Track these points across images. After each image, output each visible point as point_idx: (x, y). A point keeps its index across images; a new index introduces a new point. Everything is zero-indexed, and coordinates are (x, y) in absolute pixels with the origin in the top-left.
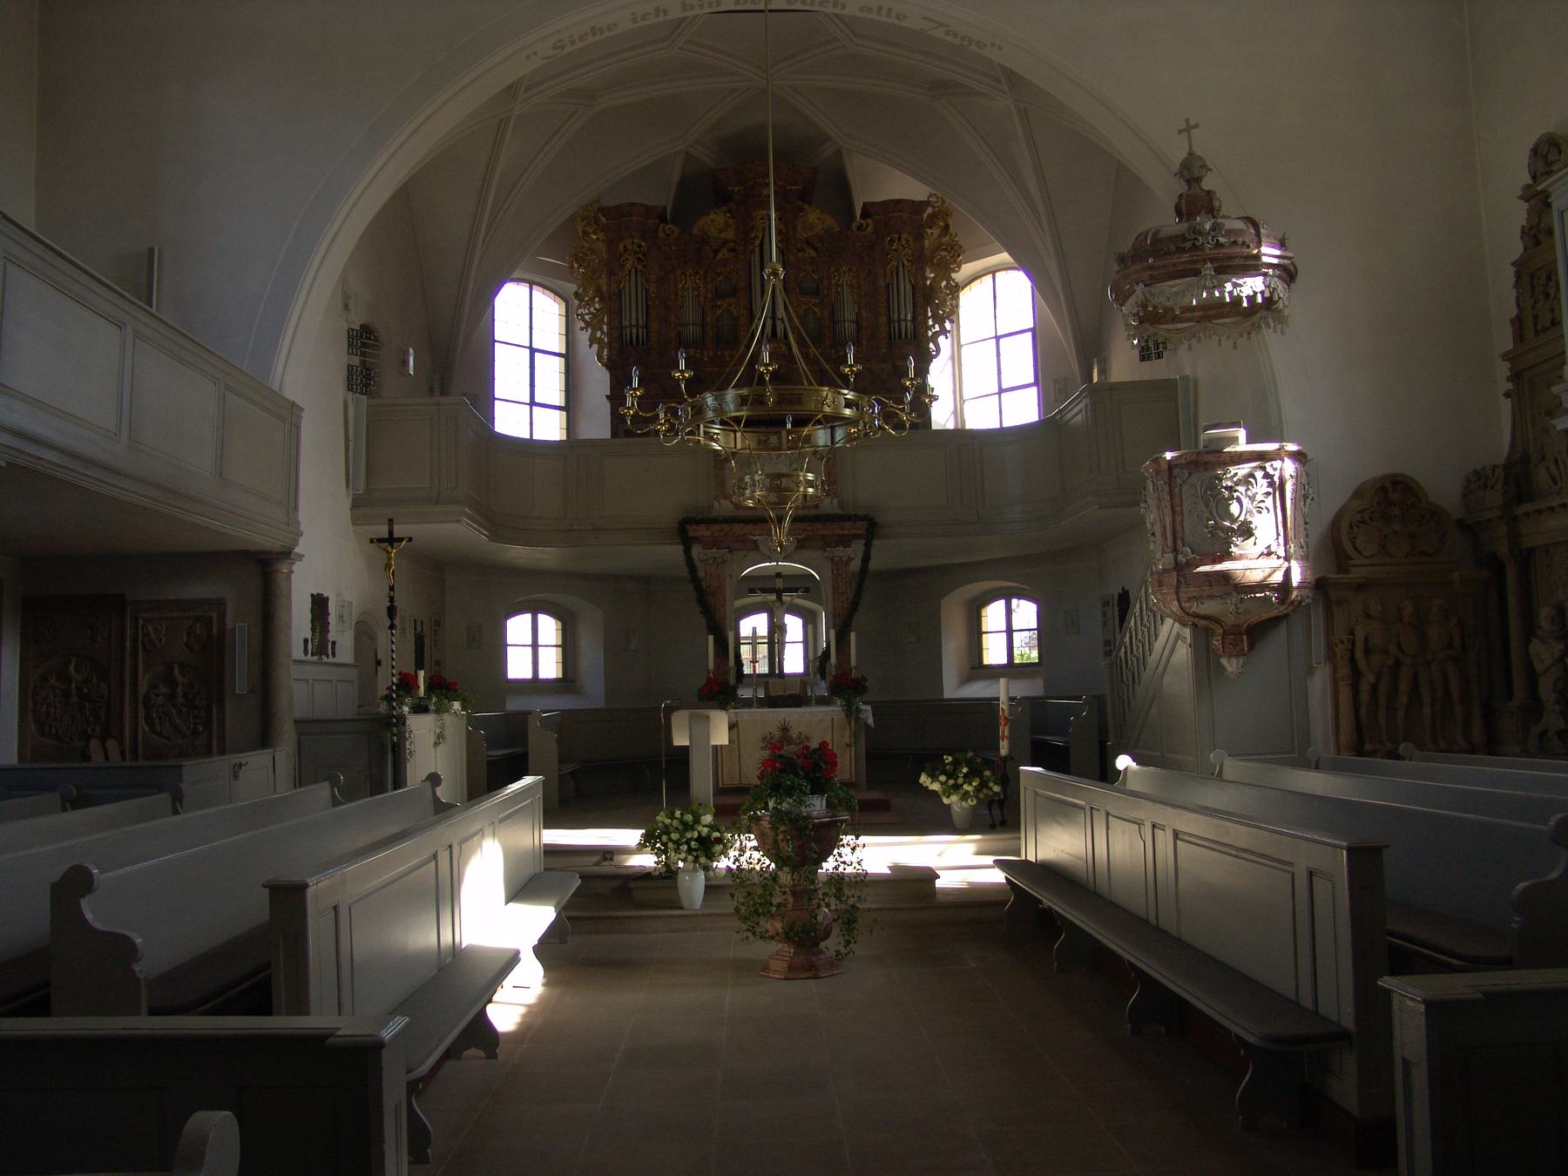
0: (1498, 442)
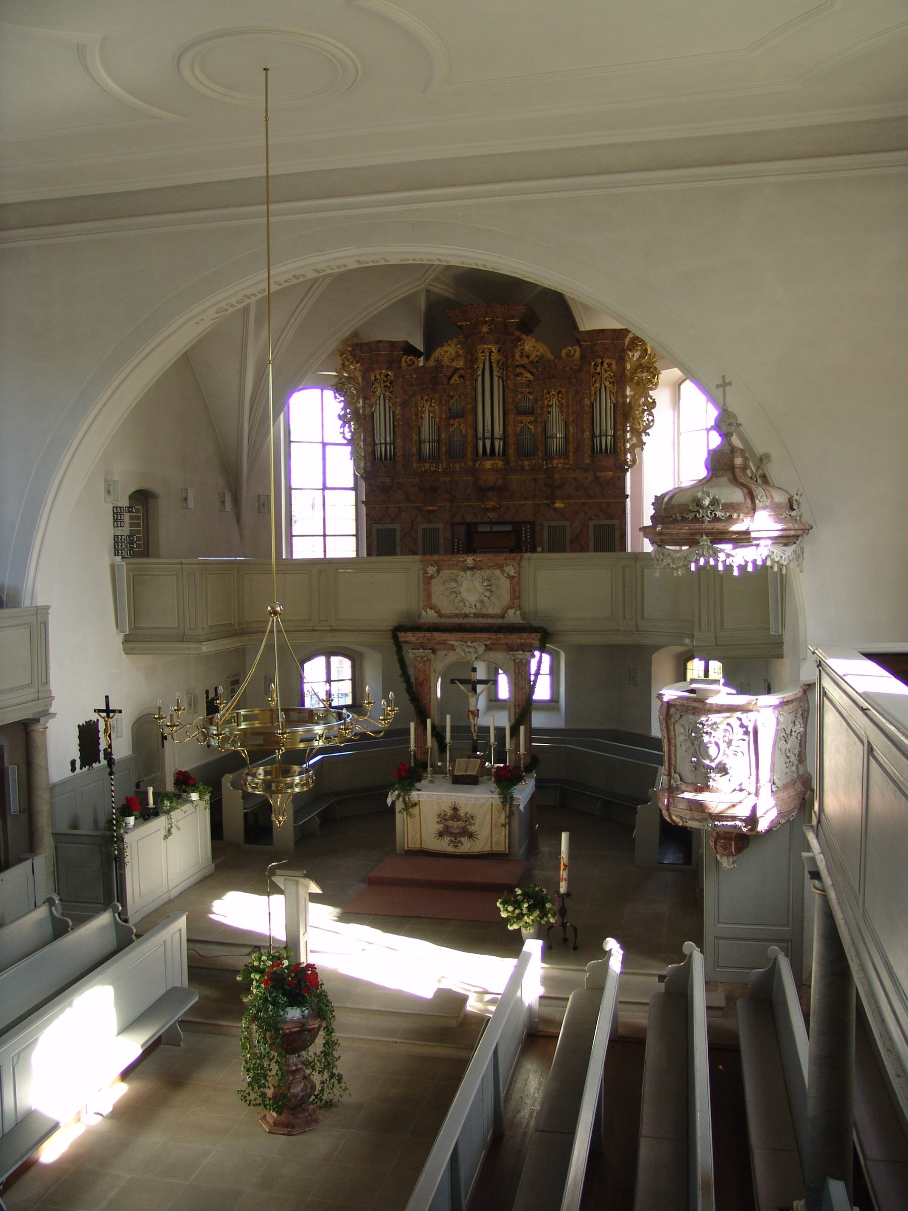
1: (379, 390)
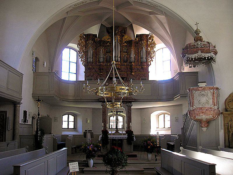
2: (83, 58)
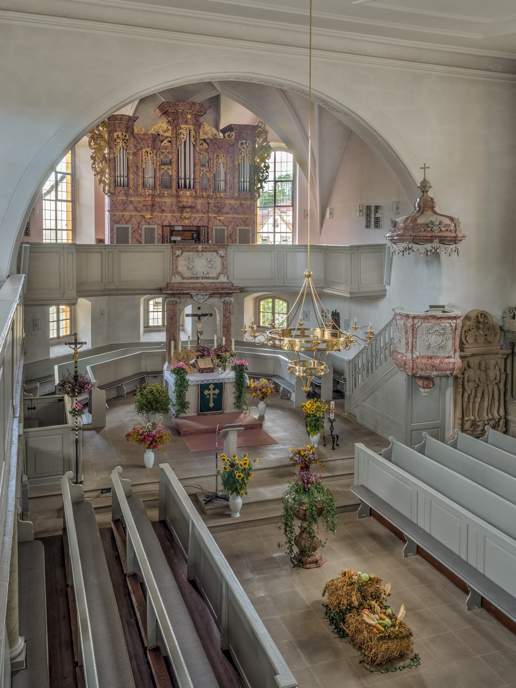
0: (437, 209)
1: (121, 144)
2: (105, 176)
